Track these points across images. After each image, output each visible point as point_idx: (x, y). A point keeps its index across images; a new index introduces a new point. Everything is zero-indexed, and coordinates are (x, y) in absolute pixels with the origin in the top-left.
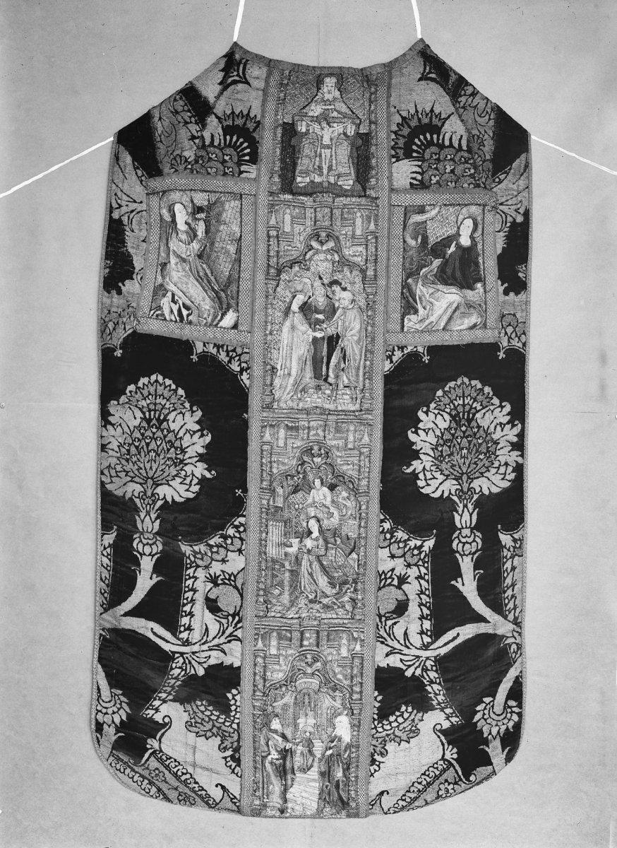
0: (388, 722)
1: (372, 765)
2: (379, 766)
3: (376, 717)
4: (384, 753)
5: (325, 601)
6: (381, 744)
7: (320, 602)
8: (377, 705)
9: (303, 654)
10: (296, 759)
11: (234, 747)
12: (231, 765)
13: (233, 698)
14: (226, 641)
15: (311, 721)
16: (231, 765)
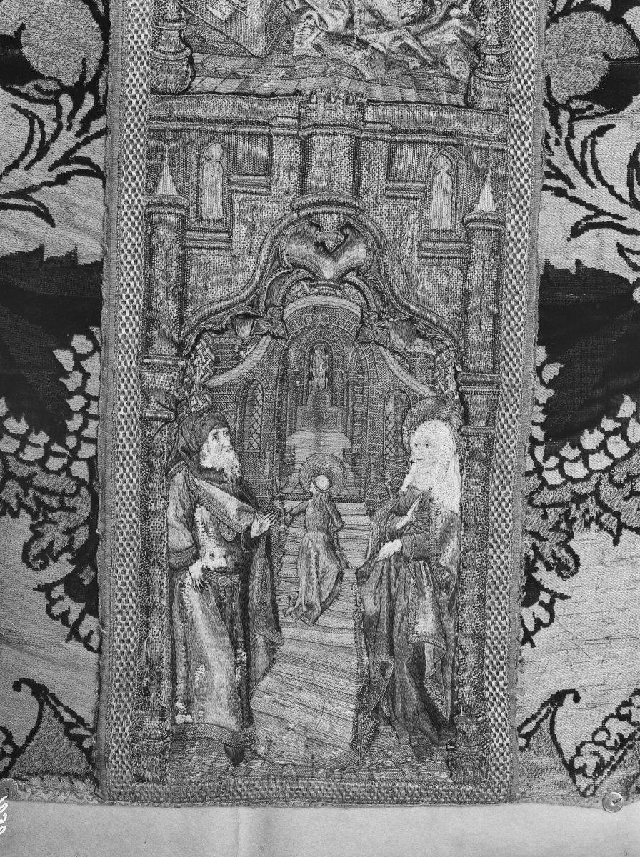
0: (577, 452)
1: (527, 603)
2: (549, 608)
3: (539, 434)
4: (566, 567)
5: (382, 40)
6: (556, 528)
7: (364, 44)
8: (544, 395)
9: (307, 216)
10: (284, 572)
11: (76, 546)
12: (67, 612)
13: (78, 367)
14: (52, 177)
15: (336, 441)
16: (67, 612)
